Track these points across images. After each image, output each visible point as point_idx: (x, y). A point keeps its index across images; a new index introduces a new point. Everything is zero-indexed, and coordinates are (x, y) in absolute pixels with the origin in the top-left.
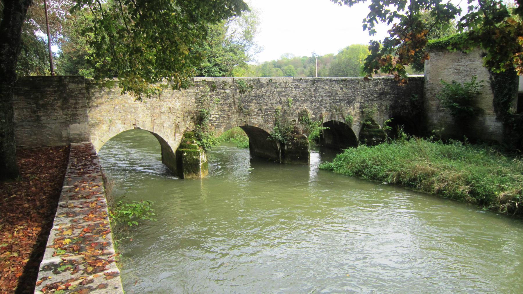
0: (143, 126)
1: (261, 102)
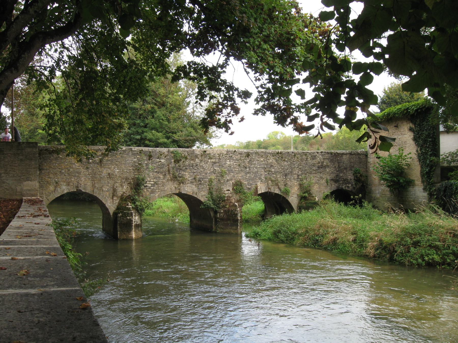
0: (84, 189)
1: (195, 171)
